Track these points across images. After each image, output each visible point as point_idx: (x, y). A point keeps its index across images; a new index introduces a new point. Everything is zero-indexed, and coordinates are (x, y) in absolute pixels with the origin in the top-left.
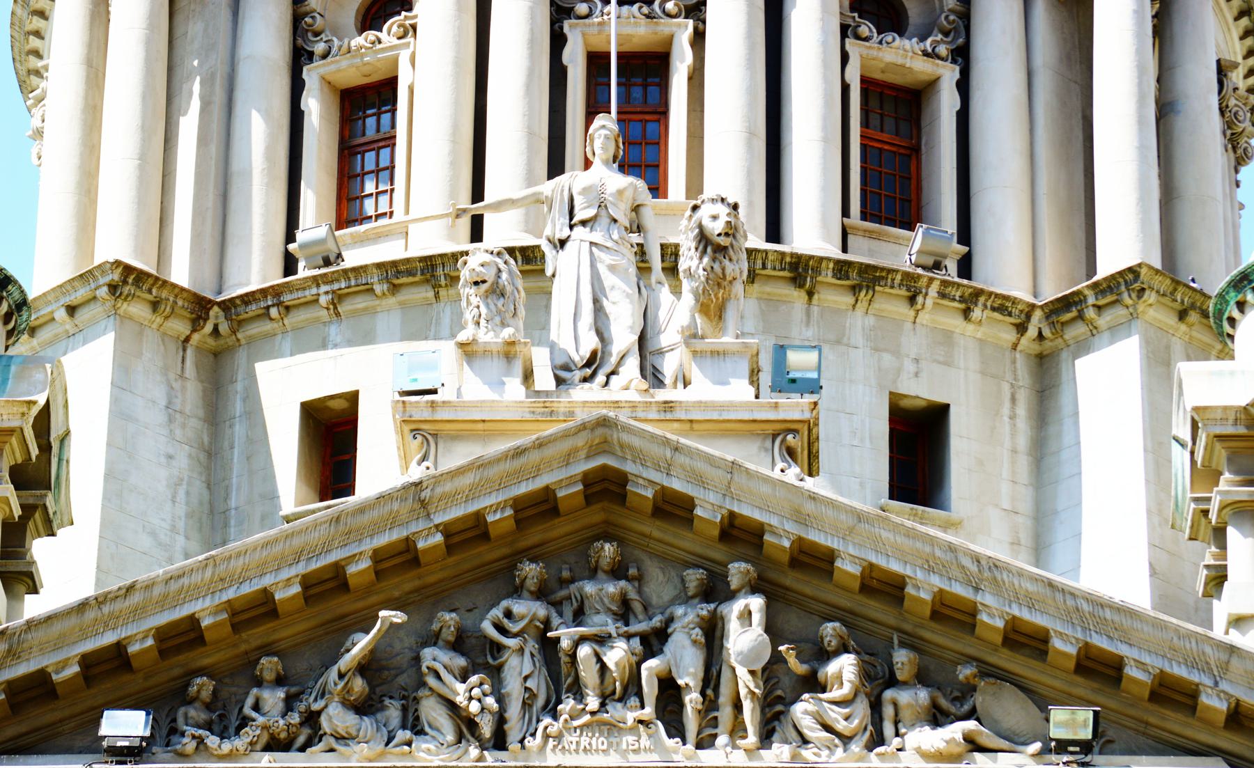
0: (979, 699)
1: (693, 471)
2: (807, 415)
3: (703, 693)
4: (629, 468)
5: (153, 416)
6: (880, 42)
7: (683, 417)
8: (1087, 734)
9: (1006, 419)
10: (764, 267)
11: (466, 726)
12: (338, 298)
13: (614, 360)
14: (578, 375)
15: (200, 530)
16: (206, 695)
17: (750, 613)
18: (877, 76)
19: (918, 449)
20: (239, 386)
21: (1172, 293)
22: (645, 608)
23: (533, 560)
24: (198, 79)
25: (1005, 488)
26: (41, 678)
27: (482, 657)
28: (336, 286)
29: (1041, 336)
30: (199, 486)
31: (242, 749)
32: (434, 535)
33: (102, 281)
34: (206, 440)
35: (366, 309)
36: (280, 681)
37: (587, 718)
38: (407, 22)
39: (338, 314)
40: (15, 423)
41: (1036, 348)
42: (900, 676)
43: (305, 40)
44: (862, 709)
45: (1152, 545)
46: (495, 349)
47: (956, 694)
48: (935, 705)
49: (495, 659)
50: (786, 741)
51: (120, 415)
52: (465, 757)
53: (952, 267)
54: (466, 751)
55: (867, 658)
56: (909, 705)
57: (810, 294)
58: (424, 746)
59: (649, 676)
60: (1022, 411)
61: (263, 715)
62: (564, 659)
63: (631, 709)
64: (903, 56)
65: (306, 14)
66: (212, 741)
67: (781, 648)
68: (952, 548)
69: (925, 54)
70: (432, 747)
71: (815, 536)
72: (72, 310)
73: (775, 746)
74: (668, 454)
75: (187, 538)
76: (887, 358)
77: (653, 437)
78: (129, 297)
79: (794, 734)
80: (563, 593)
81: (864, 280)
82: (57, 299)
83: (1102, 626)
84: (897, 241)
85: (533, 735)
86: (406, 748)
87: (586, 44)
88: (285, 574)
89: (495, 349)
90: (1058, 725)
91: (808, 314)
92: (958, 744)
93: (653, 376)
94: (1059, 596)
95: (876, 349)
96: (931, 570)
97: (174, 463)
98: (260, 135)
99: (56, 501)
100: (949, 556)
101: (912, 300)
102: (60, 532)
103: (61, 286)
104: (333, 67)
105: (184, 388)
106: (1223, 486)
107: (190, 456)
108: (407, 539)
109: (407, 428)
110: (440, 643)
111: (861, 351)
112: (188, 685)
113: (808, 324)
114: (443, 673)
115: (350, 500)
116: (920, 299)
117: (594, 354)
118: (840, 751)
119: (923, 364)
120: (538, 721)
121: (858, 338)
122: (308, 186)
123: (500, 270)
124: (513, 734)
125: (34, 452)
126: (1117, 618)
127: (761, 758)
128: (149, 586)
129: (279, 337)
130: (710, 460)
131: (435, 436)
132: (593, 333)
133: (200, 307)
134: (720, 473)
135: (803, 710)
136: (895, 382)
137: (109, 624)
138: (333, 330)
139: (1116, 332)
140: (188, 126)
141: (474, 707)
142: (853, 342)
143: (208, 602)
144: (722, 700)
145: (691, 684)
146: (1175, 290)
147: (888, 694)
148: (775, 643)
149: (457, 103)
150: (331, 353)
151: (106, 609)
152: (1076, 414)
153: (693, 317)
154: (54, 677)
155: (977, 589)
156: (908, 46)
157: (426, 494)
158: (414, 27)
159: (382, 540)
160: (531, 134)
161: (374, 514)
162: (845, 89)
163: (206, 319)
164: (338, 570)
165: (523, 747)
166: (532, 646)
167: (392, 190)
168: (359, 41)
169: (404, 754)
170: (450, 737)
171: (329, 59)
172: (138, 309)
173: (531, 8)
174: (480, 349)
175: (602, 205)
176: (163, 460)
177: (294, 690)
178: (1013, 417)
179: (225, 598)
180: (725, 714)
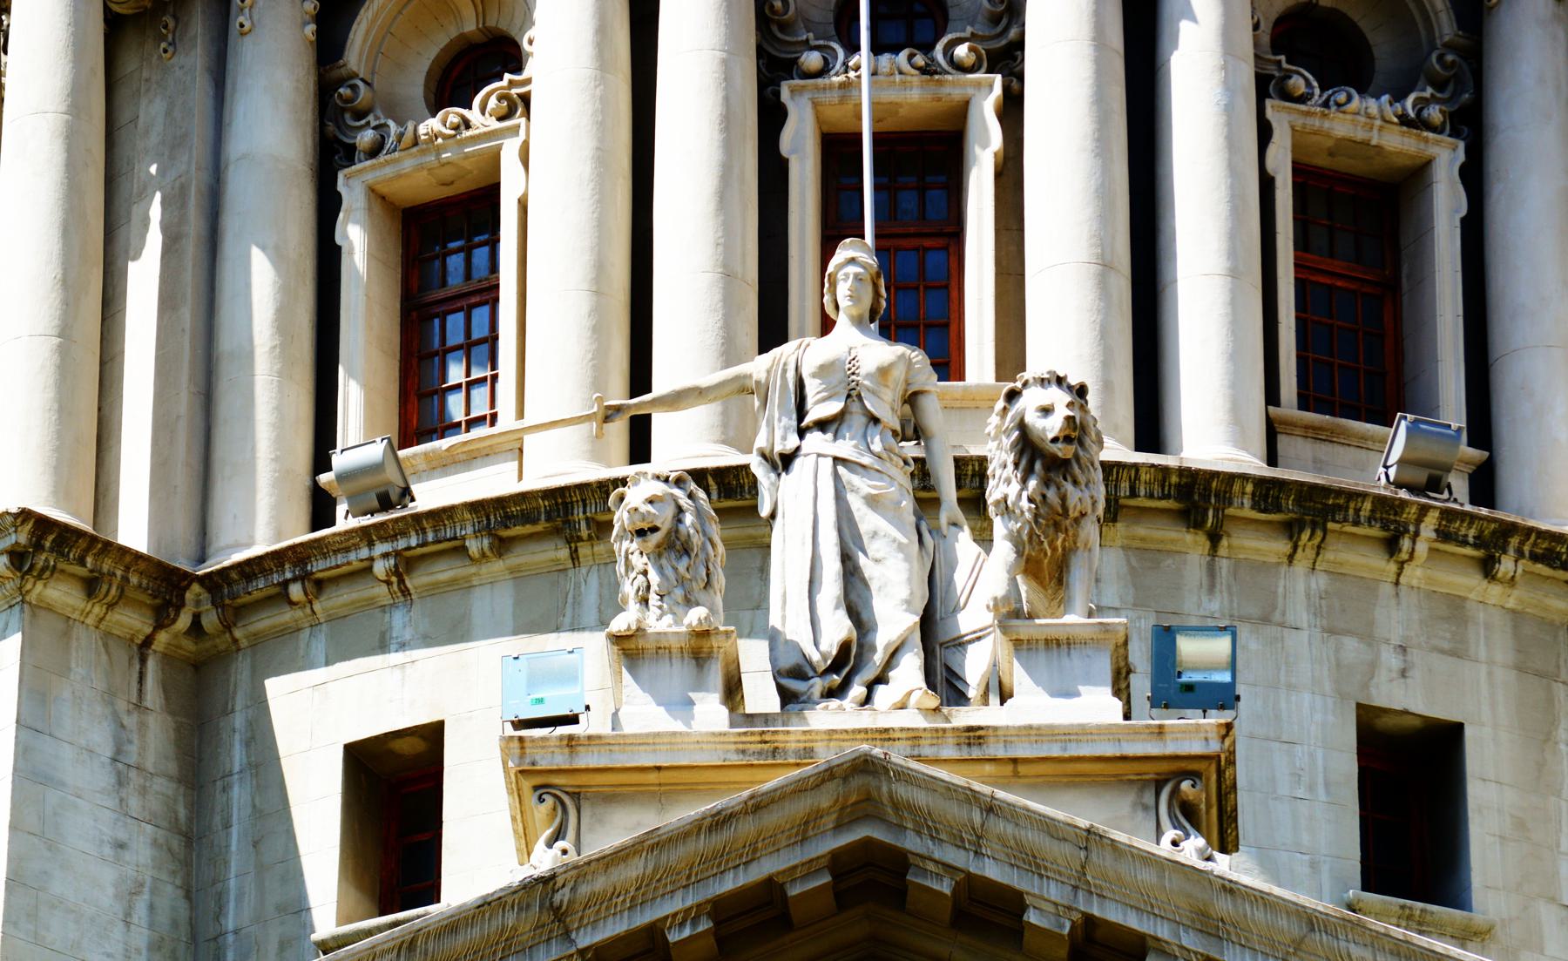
1: (1020, 846)
2: (1214, 747)
4: (911, 843)
5: (85, 772)
6: (1326, 104)
10: (1134, 493)
12: (405, 564)
13: (879, 658)
14: (818, 685)
18: (1322, 161)
20: (239, 720)
24: (158, 196)
28: (401, 544)
30: (170, 894)
34: (182, 813)
35: (452, 582)
39: (405, 592)
46: (675, 644)
53: (1459, 486)
57: (1215, 538)
64: (1366, 124)
65: (342, 81)
69: (1404, 120)
74: (977, 817)
76: (1351, 647)
77: (950, 788)
81: (1305, 512)
84: (1363, 443)
87: (819, 120)
89: (675, 644)
91: (1212, 571)
93: (946, 684)
95: (1331, 631)
97: (127, 856)
98: (264, 288)
101: (1391, 546)
104: (388, 171)
105: (142, 726)
107: (154, 843)
109: (527, 784)
113: (1212, 588)
116: (1406, 543)
117: (845, 647)
119: (1415, 655)
121: (1299, 613)
122: (350, 374)
123: (680, 510)
130: (1049, 827)
131: (576, 796)
132: (842, 614)
133: (164, 584)
134: (1067, 849)
136: (1365, 686)
138: (399, 620)
140: (143, 278)
153: (1013, 582)
157: (562, 897)
158: (526, 99)
160: (728, 275)
167: (495, 378)
171: (382, 158)
172: (61, 594)
173: (725, 63)
174: (650, 645)
175: (853, 395)
176: (108, 851)
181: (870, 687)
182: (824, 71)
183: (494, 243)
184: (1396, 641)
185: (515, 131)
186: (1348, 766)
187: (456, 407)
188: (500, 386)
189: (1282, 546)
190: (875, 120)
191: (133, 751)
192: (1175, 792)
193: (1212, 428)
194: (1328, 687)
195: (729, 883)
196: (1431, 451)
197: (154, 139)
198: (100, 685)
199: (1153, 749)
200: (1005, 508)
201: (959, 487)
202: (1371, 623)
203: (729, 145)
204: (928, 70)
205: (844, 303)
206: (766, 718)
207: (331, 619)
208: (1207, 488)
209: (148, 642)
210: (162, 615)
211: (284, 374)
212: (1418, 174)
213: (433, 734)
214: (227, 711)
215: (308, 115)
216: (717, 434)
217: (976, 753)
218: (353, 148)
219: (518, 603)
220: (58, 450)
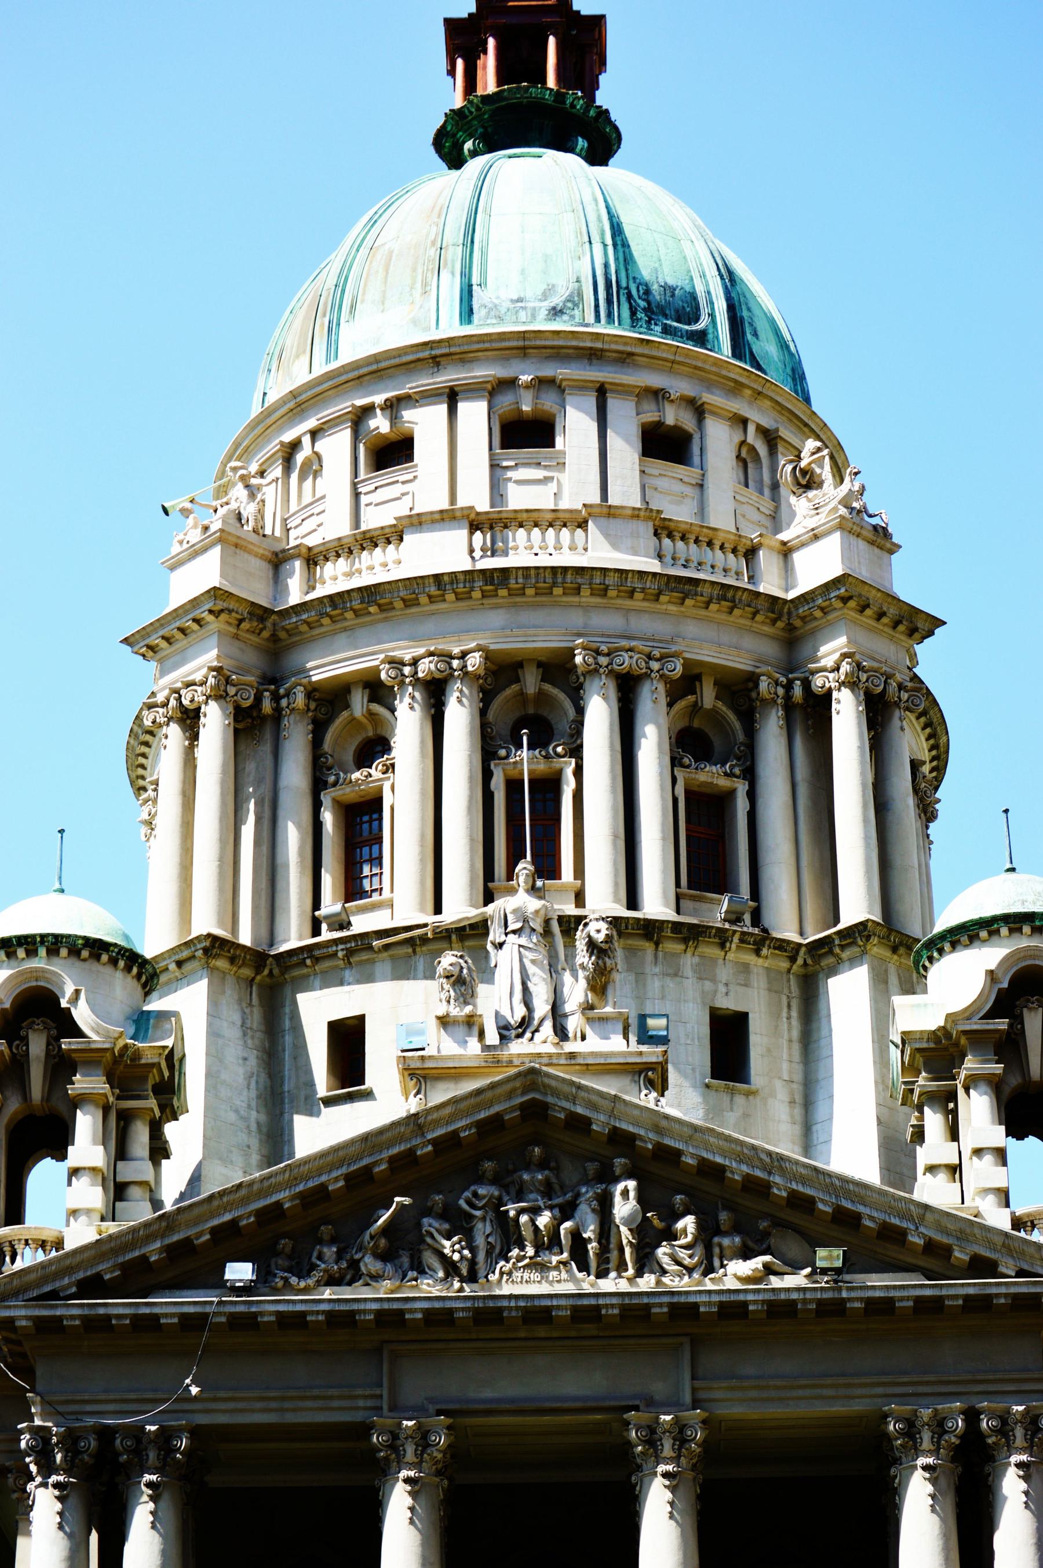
0: (772, 1241)
1: (590, 1101)
2: (661, 1059)
3: (599, 1242)
4: (550, 1099)
5: (232, 1033)
6: (697, 769)
7: (582, 1062)
8: (839, 1264)
9: (785, 1020)
10: (627, 928)
11: (451, 1268)
12: (350, 953)
13: (536, 1022)
14: (513, 1033)
15: (266, 1106)
16: (288, 1250)
17: (628, 1191)
18: (696, 789)
19: (729, 1048)
20: (287, 1010)
21: (888, 936)
22: (561, 1187)
23: (489, 1159)
24: (253, 800)
25: (785, 1066)
26: (187, 1241)
27: (460, 1225)
28: (348, 946)
29: (805, 964)
30: (263, 1076)
31: (312, 1285)
32: (427, 1146)
33: (199, 946)
34: (267, 1045)
35: (368, 960)
36: (333, 1241)
37: (527, 1261)
38: (388, 762)
39: (350, 963)
40: (156, 1060)
41: (802, 971)
42: (723, 1228)
43: (322, 773)
44: (699, 1250)
45: (878, 1104)
46: (461, 1019)
47: (758, 1237)
48: (744, 1245)
49: (468, 1223)
50: (652, 1272)
51: (213, 1034)
52: (451, 1289)
53: (747, 918)
54: (452, 1284)
55: (702, 1216)
56: (729, 1246)
57: (657, 944)
58: (426, 1281)
59: (566, 1233)
60: (794, 1014)
61: (324, 1263)
62: (511, 1223)
63: (555, 1254)
64: (711, 776)
65: (321, 756)
66: (294, 1280)
67: (649, 1215)
68: (754, 1148)
69: (726, 774)
70: (430, 1282)
71: (668, 1141)
72: (179, 964)
73: (646, 1275)
74: (574, 1090)
75: (258, 1112)
76: (708, 984)
77: (564, 1080)
78: (216, 956)
79: (657, 1267)
80: (509, 1179)
81: (690, 934)
82: (170, 957)
83: (849, 1195)
84: (711, 901)
85: (493, 1272)
86: (414, 1283)
87: (505, 775)
88: (335, 1174)
89: (461, 1019)
90: (821, 1259)
91: (656, 957)
92: (760, 1271)
93: (561, 1032)
94: (821, 1177)
95: (700, 979)
96: (741, 1161)
97: (248, 1063)
98: (293, 838)
99: (179, 1099)
100: (752, 1153)
101: (722, 946)
102: (181, 1118)
103: (172, 949)
104: (340, 792)
105: (252, 1011)
106: (921, 1081)
107: (257, 1057)
108: (410, 1149)
109: (406, 1073)
110: (433, 1214)
111: (690, 981)
112: (276, 1243)
113: (656, 963)
114: (436, 1235)
115: (362, 1087)
116: (728, 945)
117: (523, 1018)
118: (686, 1278)
119: (731, 987)
120: (497, 1263)
121: (688, 972)
122: (326, 871)
123: (462, 968)
124: (482, 1273)
125: (166, 1074)
126: (856, 1189)
127: (638, 1286)
128: (251, 1184)
129: (312, 978)
130: (600, 1094)
131: (424, 1078)
132: (522, 1005)
133: (257, 958)
134: (607, 1102)
135: (662, 1252)
136: (713, 1000)
137: (227, 1208)
138: (347, 973)
139: (854, 962)
140: (248, 831)
141: (456, 1257)
142: (685, 974)
143: (286, 1194)
144: (612, 1246)
145: (592, 1237)
146: (890, 934)
147: (716, 1240)
148: (645, 1211)
149: (423, 819)
150: (346, 988)
151: (225, 1199)
152: (829, 1015)
153: (586, 995)
154: (195, 1242)
155: (770, 1173)
156: (714, 771)
157: (421, 1120)
158: (393, 765)
159: (395, 1150)
160: (472, 840)
161: (389, 1134)
162: (675, 801)
163: (265, 966)
164: (368, 1169)
165: (488, 1281)
166: (491, 1215)
167: (381, 873)
168: (356, 775)
169: (413, 1286)
170: (441, 1274)
171: (338, 787)
172: (221, 963)
173: (470, 756)
174: (451, 1020)
175: (525, 921)
176: (241, 1061)
177: (342, 1245)
178: (789, 1018)
179: (297, 1190)
180: (614, 1255)
181: (533, 1033)
182: (507, 757)
183: (380, 819)
184: (724, 981)
185: (388, 778)
186: (706, 1030)
187: (366, 885)
188: (384, 877)
189: (682, 947)
190: (529, 775)
191: (249, 1022)
192: (646, 1075)
193: (656, 904)
194: (699, 1001)
195: (483, 1115)
196: (738, 908)
197: (251, 778)
198: (236, 997)
199: (638, 1060)
200: (583, 967)
201: (560, 926)
202: (715, 975)
203: (471, 789)
204: (547, 757)
205: (522, 884)
206: (494, 1047)
207: (322, 972)
208: (654, 926)
209: (253, 979)
210: (258, 970)
211: (302, 873)
212: (731, 793)
213: (361, 1019)
214: (283, 1006)
215: (309, 770)
216: (468, 903)
217: (573, 1062)
218: (326, 782)
219: (392, 969)
220: (219, 906)
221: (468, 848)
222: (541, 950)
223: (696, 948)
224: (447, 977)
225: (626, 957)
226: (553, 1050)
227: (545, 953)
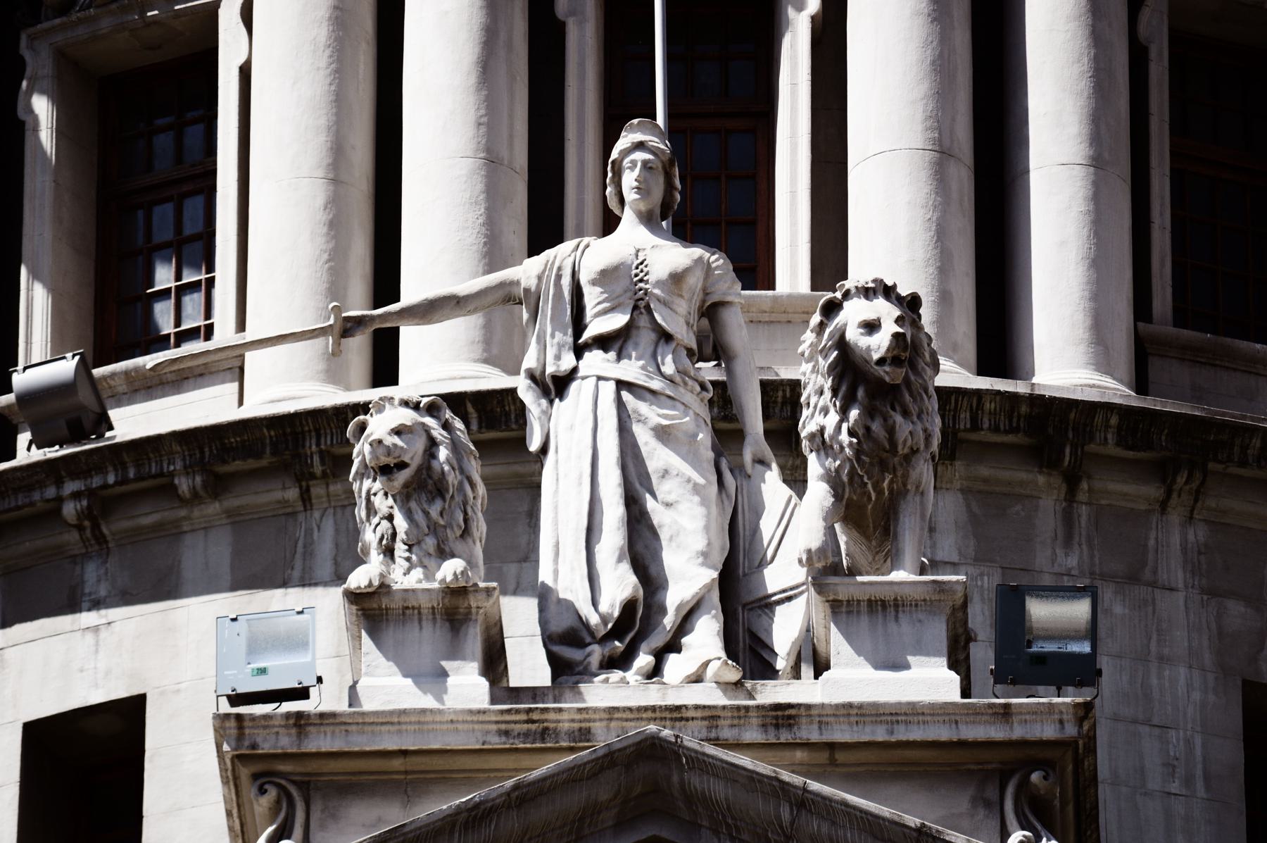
2: (1071, 730)
7: (815, 737)
10: (975, 426)
12: (101, 506)
13: (669, 621)
14: (596, 653)
28: (96, 482)
35: (158, 527)
39: (101, 539)
46: (425, 603)
57: (1072, 481)
74: (785, 813)
77: (753, 778)
89: (425, 603)
91: (1068, 520)
104: (82, 32)
111: (1180, 597)
117: (629, 607)
122: (35, 275)
123: (433, 443)
142: (1163, 577)
153: (830, 531)
167: (211, 282)
174: (396, 604)
175: (641, 307)
181: (660, 656)
188: (217, 292)
189: (1153, 491)
194: (1208, 659)
199: (996, 733)
200: (822, 443)
205: (630, 196)
206: (534, 693)
216: (478, 351)
217: (785, 736)
221: (480, 186)
222: (689, 398)
223: (1197, 495)
224: (385, 471)
225: (974, 520)
226: (717, 698)
227: (704, 412)
